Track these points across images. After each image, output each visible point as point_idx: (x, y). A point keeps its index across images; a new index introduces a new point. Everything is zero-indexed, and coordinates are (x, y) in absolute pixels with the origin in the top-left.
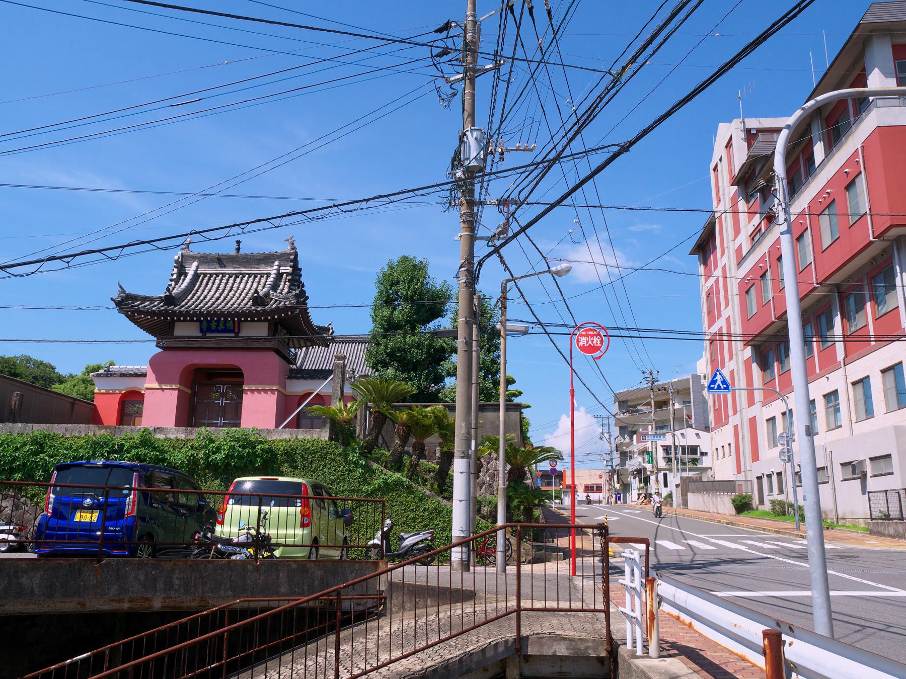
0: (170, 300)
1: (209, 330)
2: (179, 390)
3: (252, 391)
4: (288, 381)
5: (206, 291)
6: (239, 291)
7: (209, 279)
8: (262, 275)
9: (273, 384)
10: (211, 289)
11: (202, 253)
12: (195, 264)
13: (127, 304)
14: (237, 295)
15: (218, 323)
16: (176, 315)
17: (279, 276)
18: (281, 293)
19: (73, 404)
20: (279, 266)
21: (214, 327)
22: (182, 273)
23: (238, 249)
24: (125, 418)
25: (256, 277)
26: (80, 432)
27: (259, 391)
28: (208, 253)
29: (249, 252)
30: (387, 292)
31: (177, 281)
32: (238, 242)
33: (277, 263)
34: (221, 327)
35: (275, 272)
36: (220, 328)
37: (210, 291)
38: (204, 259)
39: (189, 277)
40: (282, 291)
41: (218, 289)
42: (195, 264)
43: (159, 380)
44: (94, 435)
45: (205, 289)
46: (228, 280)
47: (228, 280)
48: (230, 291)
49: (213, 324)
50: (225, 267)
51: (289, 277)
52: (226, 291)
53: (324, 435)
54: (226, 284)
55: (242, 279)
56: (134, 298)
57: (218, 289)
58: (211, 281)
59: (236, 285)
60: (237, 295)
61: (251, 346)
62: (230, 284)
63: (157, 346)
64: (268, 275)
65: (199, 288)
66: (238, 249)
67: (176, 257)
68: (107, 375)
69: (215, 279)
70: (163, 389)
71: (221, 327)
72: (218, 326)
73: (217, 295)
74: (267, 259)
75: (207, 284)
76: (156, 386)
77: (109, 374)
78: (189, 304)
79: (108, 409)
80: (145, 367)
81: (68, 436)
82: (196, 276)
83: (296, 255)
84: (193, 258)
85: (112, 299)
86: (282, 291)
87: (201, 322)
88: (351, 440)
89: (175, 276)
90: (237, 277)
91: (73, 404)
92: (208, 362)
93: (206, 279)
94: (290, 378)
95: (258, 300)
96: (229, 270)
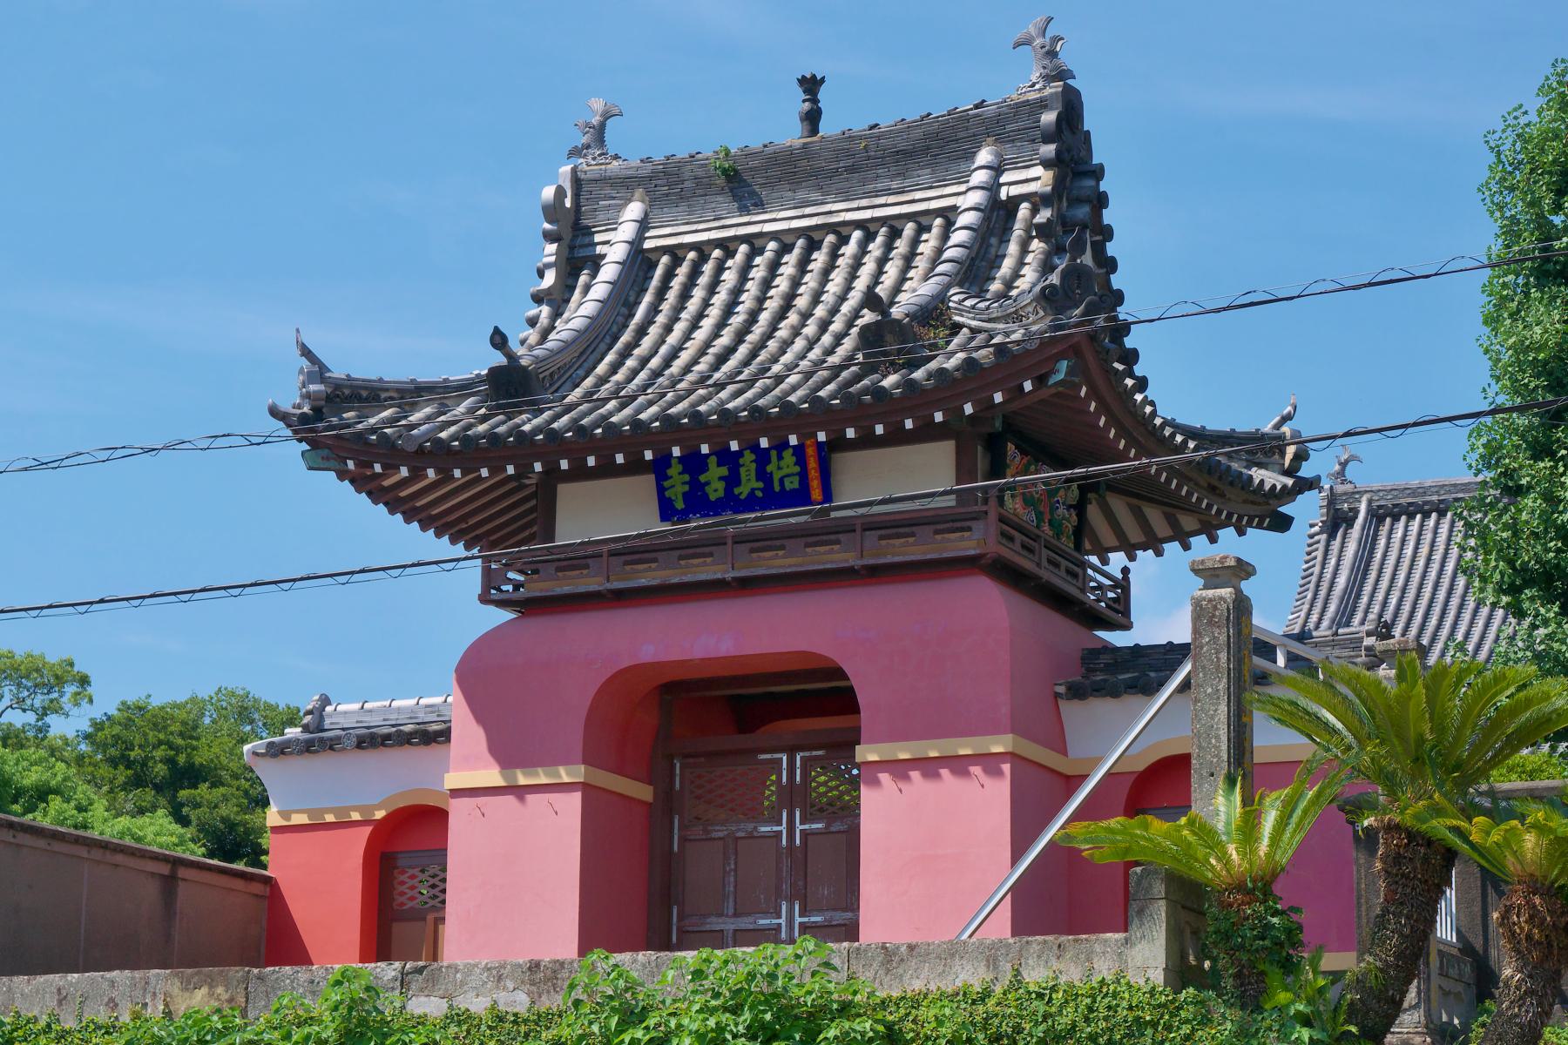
0: (510, 384)
1: (697, 502)
2: (586, 788)
3: (899, 769)
4: (1072, 712)
5: (679, 328)
6: (820, 311)
7: (695, 272)
8: (922, 222)
9: (993, 729)
10: (700, 315)
11: (659, 157)
12: (634, 210)
13: (343, 428)
14: (810, 329)
15: (738, 478)
16: (593, 445)
17: (998, 214)
18: (1003, 296)
19: (169, 883)
20: (997, 169)
21: (716, 490)
22: (578, 259)
23: (812, 118)
24: (398, 929)
25: (895, 234)
26: (113, 1004)
27: (930, 767)
28: (682, 154)
29: (859, 125)
30: (1542, 224)
31: (558, 300)
32: (811, 85)
33: (984, 156)
34: (749, 484)
35: (976, 198)
36: (743, 491)
37: (695, 325)
38: (669, 185)
39: (608, 272)
40: (1009, 284)
41: (729, 311)
42: (634, 210)
43: (505, 753)
44: (168, 1014)
45: (675, 319)
46: (774, 266)
47: (774, 266)
48: (781, 315)
49: (714, 476)
50: (760, 205)
51: (1044, 215)
52: (764, 317)
53: (1141, 958)
54: (767, 284)
55: (834, 255)
56: (367, 395)
57: (729, 311)
58: (703, 280)
59: (810, 281)
60: (810, 329)
61: (892, 556)
62: (782, 284)
63: (485, 599)
64: (948, 215)
65: (649, 321)
66: (812, 118)
67: (548, 193)
68: (307, 748)
69: (720, 268)
70: (519, 792)
71: (749, 484)
72: (732, 480)
73: (725, 340)
74: (939, 145)
75: (685, 295)
76: (492, 776)
77: (320, 740)
78: (616, 395)
79: (322, 886)
80: (440, 697)
81: (70, 1024)
82: (639, 262)
83: (1071, 107)
84: (625, 185)
85: (274, 412)
86: (1009, 284)
87: (660, 467)
88: (1275, 976)
89: (550, 278)
90: (813, 246)
91: (169, 883)
92: (675, 655)
93: (683, 271)
94: (1077, 692)
95: (887, 338)
96: (779, 219)
